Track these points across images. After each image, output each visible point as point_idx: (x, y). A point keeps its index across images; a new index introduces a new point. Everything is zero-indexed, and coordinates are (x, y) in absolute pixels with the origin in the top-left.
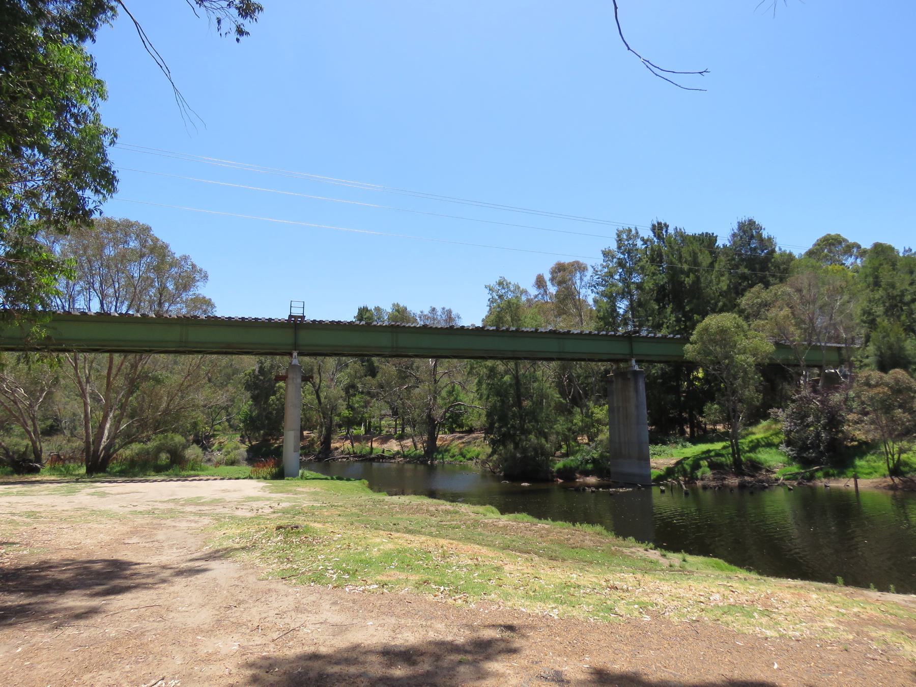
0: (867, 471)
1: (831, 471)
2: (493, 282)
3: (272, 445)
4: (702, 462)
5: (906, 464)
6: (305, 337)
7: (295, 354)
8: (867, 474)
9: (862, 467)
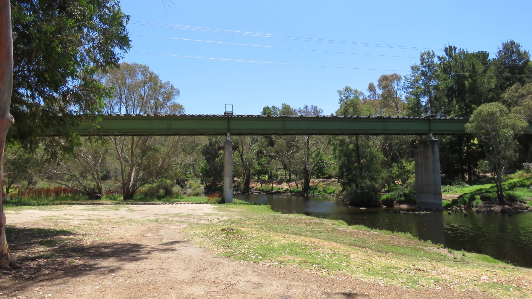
2: (342, 89)
4: (476, 196)
6: (234, 125)
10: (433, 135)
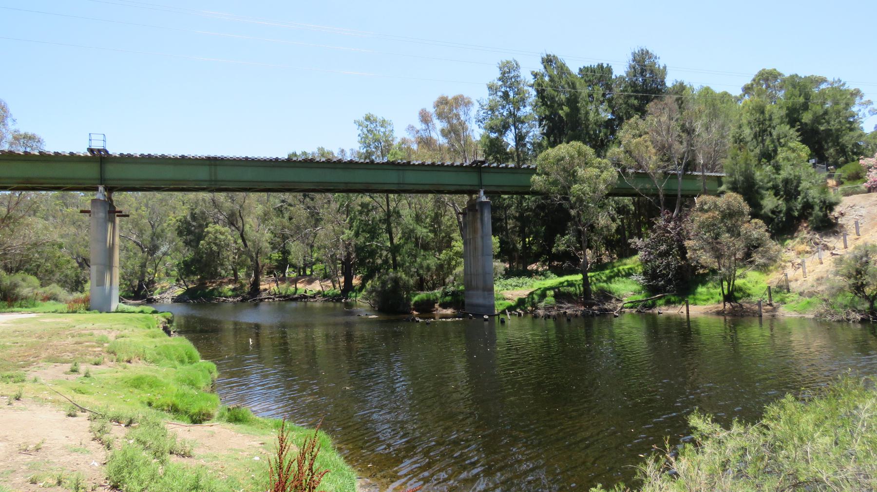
0: (704, 298)
1: (673, 299)
2: (361, 118)
3: (207, 288)
4: (548, 292)
5: (740, 289)
7: (101, 188)
8: (705, 300)
9: (701, 294)
10: (485, 193)
